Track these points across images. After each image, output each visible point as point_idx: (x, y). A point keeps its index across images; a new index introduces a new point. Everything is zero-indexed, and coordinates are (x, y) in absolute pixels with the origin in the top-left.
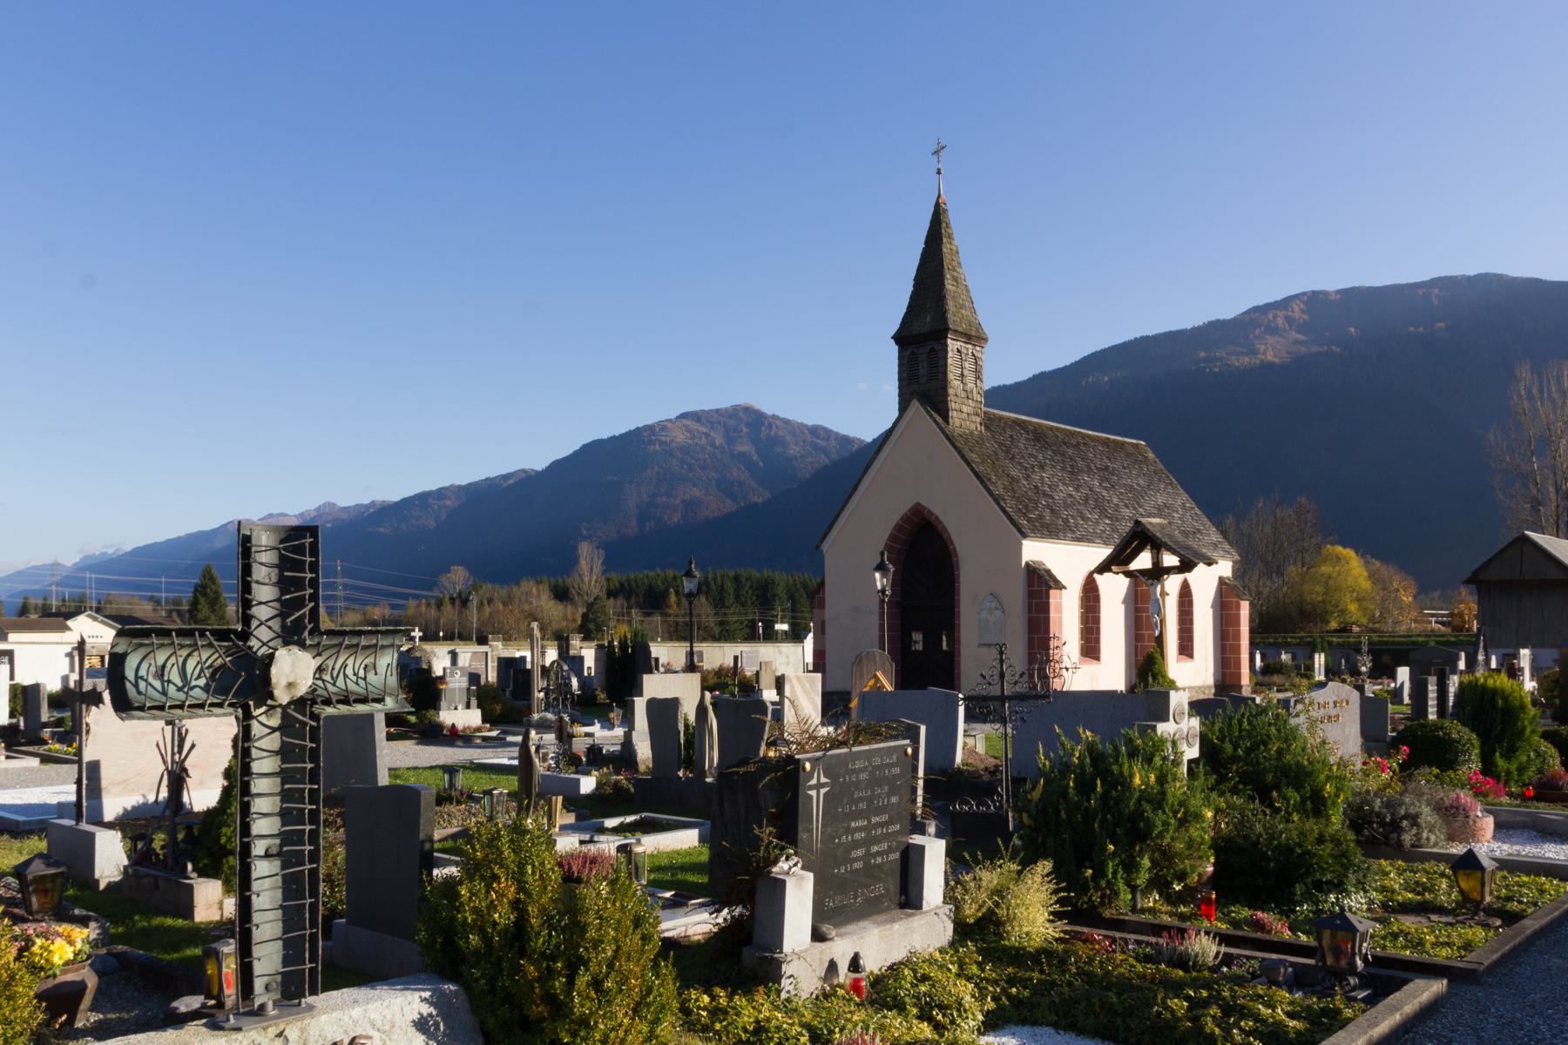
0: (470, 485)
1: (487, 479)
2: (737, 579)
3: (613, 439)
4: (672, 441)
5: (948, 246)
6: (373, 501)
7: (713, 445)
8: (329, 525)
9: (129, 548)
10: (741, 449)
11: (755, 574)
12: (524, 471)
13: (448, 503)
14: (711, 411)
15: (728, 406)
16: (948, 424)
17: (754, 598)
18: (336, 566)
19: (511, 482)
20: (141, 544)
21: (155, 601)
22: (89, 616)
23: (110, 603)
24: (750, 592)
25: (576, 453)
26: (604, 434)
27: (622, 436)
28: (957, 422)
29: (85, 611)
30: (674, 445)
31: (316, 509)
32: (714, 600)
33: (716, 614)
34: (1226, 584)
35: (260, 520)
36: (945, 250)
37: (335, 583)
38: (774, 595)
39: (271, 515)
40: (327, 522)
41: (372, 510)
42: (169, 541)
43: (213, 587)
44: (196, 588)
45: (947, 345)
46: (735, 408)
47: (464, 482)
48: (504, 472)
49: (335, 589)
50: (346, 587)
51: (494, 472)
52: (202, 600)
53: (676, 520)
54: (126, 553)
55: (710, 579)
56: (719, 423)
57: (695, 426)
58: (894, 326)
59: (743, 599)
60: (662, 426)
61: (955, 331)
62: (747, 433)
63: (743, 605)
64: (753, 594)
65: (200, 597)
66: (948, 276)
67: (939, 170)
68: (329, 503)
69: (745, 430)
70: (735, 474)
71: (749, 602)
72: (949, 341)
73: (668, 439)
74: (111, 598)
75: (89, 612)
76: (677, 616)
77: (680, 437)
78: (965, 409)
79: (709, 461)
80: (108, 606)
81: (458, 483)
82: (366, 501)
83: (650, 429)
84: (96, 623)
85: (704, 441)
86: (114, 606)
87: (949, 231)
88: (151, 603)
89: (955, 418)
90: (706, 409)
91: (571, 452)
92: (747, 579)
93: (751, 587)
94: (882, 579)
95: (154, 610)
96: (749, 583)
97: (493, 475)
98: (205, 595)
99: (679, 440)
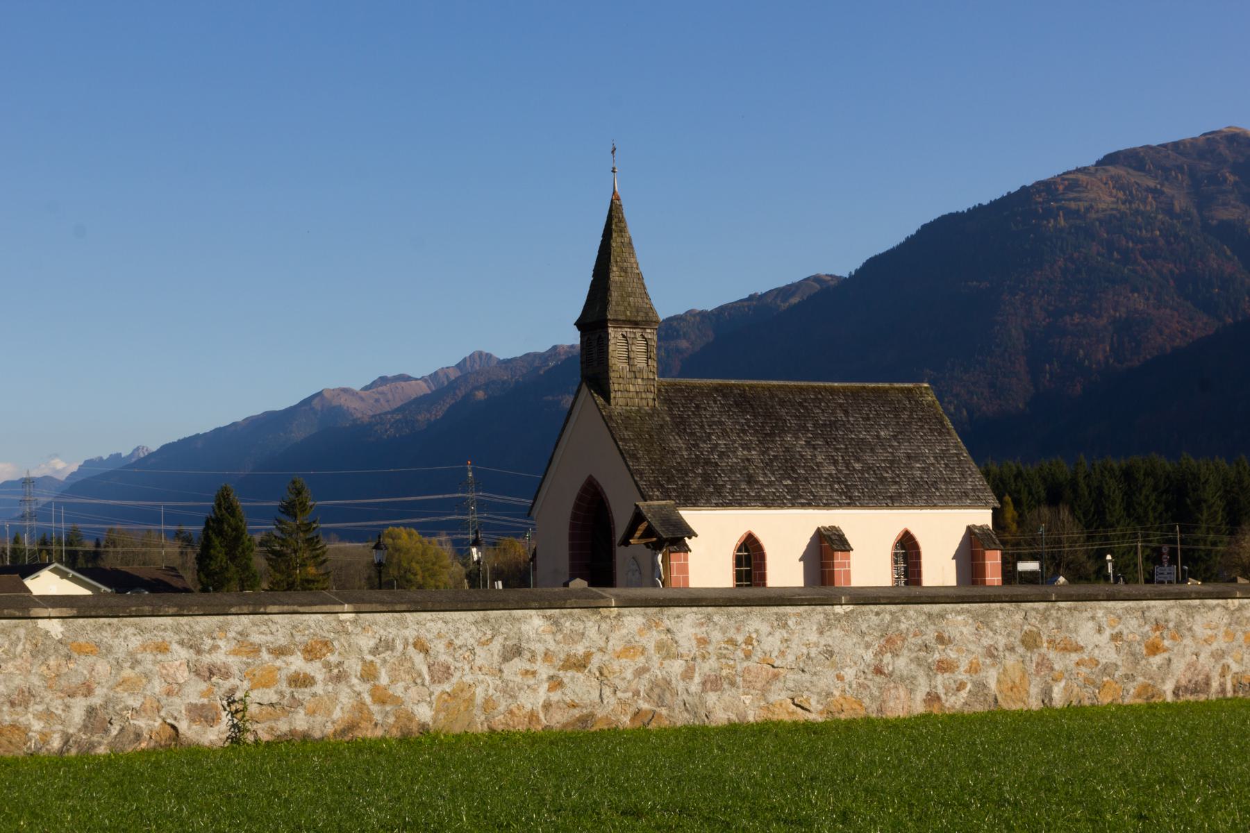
0: (722, 309)
1: (751, 298)
2: (1128, 475)
3: (978, 211)
4: (1089, 209)
5: (619, 240)
6: (555, 347)
7: (1170, 211)
8: (480, 395)
9: (154, 447)
10: (1224, 214)
11: (1165, 464)
12: (817, 279)
13: (684, 344)
14: (1164, 146)
15: (1197, 135)
16: (609, 404)
17: (1161, 508)
18: (466, 471)
19: (795, 300)
20: (174, 438)
21: (184, 539)
22: (55, 571)
23: (114, 544)
24: (1153, 497)
25: (910, 241)
26: (962, 203)
27: (994, 205)
28: (622, 402)
29: (50, 563)
30: (1093, 215)
31: (458, 366)
32: (1085, 515)
33: (1089, 538)
34: (975, 534)
35: (366, 388)
36: (614, 244)
37: (465, 499)
38: (1198, 503)
39: (383, 380)
40: (477, 388)
41: (551, 364)
42: (218, 431)
43: (232, 521)
44: (207, 523)
45: (608, 334)
46: (1211, 139)
47: (710, 306)
48: (781, 283)
49: (465, 510)
50: (481, 506)
51: (762, 286)
52: (216, 542)
53: (1100, 356)
54: (152, 455)
55: (1081, 479)
56: (1180, 168)
57: (1134, 177)
58: (577, 312)
59: (1140, 510)
60: (1071, 182)
61: (616, 321)
62: (1236, 183)
63: (1139, 520)
64: (1158, 502)
65: (213, 536)
66: (615, 269)
67: (614, 168)
68: (480, 354)
69: (1231, 178)
70: (1215, 266)
71: (1151, 514)
72: (611, 330)
73: (1082, 205)
74: (114, 536)
75: (56, 565)
76: (1018, 544)
77: (1105, 200)
78: (631, 388)
79: (1162, 242)
80: (111, 549)
81: (700, 307)
82: (542, 347)
83: (1045, 187)
84: (65, 581)
85: (1151, 204)
86: (119, 549)
87: (623, 225)
88: (180, 543)
89: (618, 398)
90: (1154, 143)
91: (902, 239)
92: (1146, 474)
93: (1155, 489)
94: (477, 554)
95: (182, 553)
96: (1150, 481)
97: (762, 289)
98: (220, 533)
99: (1102, 206)
